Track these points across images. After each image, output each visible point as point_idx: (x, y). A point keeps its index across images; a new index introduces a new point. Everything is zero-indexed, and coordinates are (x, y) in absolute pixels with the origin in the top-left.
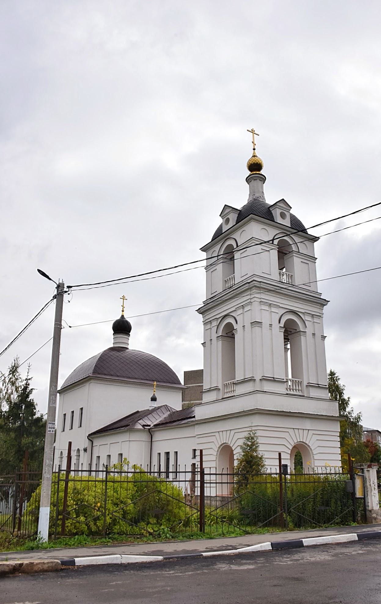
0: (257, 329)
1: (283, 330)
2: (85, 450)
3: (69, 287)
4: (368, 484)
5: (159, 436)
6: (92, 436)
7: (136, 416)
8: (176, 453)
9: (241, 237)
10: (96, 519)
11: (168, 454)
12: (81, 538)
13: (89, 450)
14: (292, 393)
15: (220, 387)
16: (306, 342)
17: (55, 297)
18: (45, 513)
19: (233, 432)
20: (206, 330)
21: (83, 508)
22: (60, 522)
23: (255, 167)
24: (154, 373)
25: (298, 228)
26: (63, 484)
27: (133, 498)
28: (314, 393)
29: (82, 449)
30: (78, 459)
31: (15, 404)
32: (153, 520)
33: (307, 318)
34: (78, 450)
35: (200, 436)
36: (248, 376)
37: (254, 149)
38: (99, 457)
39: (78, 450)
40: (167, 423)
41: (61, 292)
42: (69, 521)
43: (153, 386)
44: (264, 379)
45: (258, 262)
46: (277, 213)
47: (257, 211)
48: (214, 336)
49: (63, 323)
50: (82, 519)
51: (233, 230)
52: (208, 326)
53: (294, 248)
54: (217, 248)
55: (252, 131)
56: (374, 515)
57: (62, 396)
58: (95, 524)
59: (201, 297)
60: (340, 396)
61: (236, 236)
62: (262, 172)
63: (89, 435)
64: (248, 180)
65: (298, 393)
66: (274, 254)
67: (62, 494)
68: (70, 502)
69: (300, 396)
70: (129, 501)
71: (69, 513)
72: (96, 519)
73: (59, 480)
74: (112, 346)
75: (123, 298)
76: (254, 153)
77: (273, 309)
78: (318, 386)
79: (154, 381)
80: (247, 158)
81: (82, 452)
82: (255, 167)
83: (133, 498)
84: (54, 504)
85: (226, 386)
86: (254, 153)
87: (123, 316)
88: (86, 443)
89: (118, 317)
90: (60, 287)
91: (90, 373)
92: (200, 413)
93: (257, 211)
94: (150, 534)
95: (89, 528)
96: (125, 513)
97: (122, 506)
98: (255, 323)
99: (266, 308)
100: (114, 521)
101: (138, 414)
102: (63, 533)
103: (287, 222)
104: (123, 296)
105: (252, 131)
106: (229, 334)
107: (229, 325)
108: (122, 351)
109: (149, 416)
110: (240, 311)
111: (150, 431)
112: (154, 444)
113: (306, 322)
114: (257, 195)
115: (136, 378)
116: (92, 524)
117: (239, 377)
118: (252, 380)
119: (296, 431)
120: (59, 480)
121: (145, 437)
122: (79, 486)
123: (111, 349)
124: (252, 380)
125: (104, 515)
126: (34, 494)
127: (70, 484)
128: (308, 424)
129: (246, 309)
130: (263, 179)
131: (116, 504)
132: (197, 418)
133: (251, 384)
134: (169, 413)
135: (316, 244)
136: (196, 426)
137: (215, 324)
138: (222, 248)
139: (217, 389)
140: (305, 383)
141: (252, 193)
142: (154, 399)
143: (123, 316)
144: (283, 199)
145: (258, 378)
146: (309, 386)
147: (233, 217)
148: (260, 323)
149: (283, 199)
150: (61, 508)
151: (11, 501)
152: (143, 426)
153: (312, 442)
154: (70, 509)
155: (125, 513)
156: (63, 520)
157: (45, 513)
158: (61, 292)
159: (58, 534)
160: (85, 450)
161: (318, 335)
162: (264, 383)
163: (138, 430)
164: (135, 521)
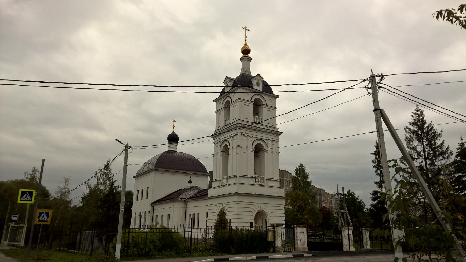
0: (239, 150)
1: (254, 150)
2: (149, 212)
3: (130, 147)
4: (276, 234)
5: (191, 204)
6: (153, 204)
7: (180, 192)
8: (198, 214)
9: (234, 97)
10: (142, 249)
11: (194, 214)
12: (135, 257)
13: (152, 212)
14: (258, 183)
15: (221, 179)
16: (267, 156)
17: (124, 150)
18: (118, 247)
19: (225, 204)
20: (215, 147)
21: (136, 245)
22: (125, 251)
23: (246, 51)
24: (192, 166)
25: (267, 89)
26: (127, 234)
27: (160, 240)
28: (271, 183)
29: (147, 211)
30: (145, 217)
31: (106, 195)
32: (169, 250)
33: (269, 142)
34: (146, 212)
35: (210, 205)
36: (234, 174)
37: (246, 40)
38: (157, 216)
39: (146, 212)
40: (192, 198)
41: (127, 148)
42: (130, 250)
43: (189, 174)
44: (242, 176)
45: (242, 111)
46: (254, 82)
47: (245, 81)
48: (219, 151)
49: (128, 163)
50: (135, 249)
51: (229, 92)
52: (216, 145)
53: (264, 103)
54: (222, 101)
55: (245, 28)
56: (278, 249)
57: (137, 179)
58: (141, 251)
59: (212, 129)
60: (306, 180)
61: (232, 95)
62: (250, 55)
63: (152, 203)
64: (241, 59)
65: (261, 184)
66: (252, 107)
67: (126, 239)
68: (130, 242)
69: (262, 185)
70: (157, 241)
71: (129, 247)
72: (142, 249)
73: (125, 233)
74: (167, 150)
75: (174, 121)
76: (246, 43)
77: (249, 138)
78: (273, 180)
79: (191, 171)
80: (240, 46)
81: (147, 213)
82: (246, 51)
83: (160, 240)
84: (123, 243)
85: (224, 179)
86: (246, 43)
87: (173, 132)
88: (150, 208)
89: (171, 132)
90: (126, 146)
91: (153, 166)
92: (211, 193)
93: (245, 81)
94: (166, 255)
95: (139, 253)
96: (155, 246)
97: (154, 243)
98: (239, 146)
99: (245, 138)
100: (150, 250)
101: (181, 191)
102: (127, 255)
103: (260, 89)
104: (174, 120)
105: (245, 28)
106: (226, 150)
107: (226, 146)
108: (173, 153)
109: (186, 193)
110: (231, 139)
111: (185, 201)
112: (188, 209)
113: (268, 145)
114: (246, 70)
115: (180, 170)
116: (140, 251)
117: (230, 175)
118: (236, 177)
119: (259, 204)
120: (125, 233)
121: (182, 205)
122: (134, 235)
123: (166, 152)
124: (236, 177)
125: (146, 247)
126: (114, 239)
127: (131, 234)
128: (266, 200)
129: (235, 138)
130: (250, 59)
131: (152, 243)
132: (209, 196)
133: (234, 179)
134: (197, 190)
135: (277, 99)
136: (208, 200)
137: (219, 144)
138: (224, 100)
139: (219, 180)
140: (266, 178)
141: (243, 68)
142: (190, 182)
143: (173, 132)
144: (259, 74)
145: (238, 176)
146: (268, 180)
147: (230, 84)
148: (242, 144)
149: (259, 74)
150: (126, 245)
151: (104, 242)
152: (182, 199)
153: (268, 210)
154: (130, 245)
155: (155, 246)
156: (127, 250)
157: (118, 247)
158: (127, 148)
159: (125, 256)
160: (149, 212)
161: (275, 151)
162: (269, 181)
163: (179, 201)
164: (159, 250)
